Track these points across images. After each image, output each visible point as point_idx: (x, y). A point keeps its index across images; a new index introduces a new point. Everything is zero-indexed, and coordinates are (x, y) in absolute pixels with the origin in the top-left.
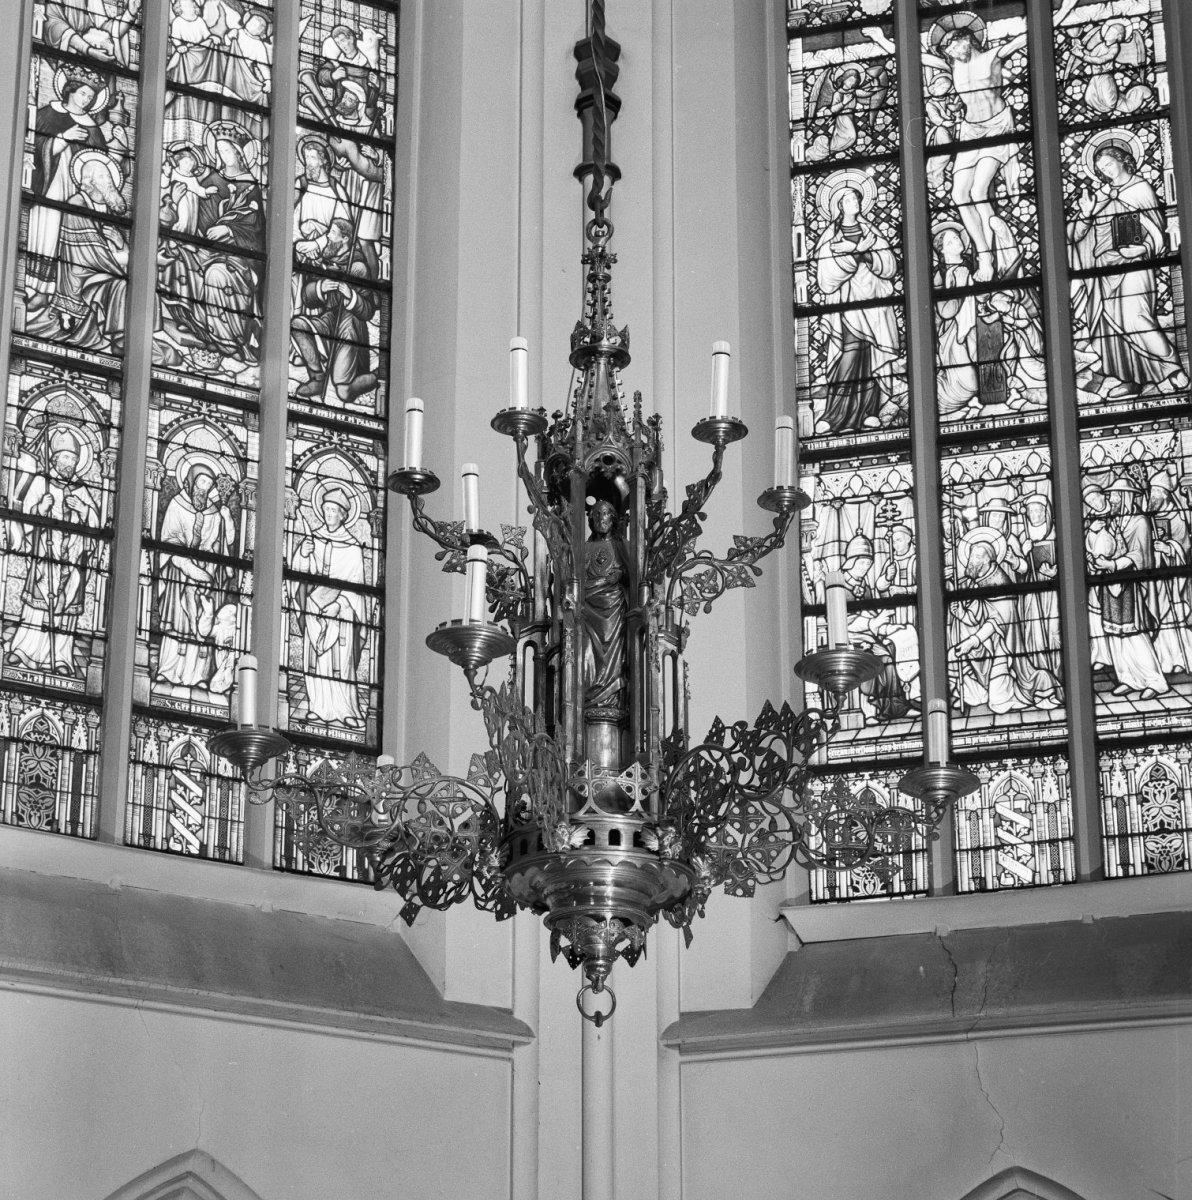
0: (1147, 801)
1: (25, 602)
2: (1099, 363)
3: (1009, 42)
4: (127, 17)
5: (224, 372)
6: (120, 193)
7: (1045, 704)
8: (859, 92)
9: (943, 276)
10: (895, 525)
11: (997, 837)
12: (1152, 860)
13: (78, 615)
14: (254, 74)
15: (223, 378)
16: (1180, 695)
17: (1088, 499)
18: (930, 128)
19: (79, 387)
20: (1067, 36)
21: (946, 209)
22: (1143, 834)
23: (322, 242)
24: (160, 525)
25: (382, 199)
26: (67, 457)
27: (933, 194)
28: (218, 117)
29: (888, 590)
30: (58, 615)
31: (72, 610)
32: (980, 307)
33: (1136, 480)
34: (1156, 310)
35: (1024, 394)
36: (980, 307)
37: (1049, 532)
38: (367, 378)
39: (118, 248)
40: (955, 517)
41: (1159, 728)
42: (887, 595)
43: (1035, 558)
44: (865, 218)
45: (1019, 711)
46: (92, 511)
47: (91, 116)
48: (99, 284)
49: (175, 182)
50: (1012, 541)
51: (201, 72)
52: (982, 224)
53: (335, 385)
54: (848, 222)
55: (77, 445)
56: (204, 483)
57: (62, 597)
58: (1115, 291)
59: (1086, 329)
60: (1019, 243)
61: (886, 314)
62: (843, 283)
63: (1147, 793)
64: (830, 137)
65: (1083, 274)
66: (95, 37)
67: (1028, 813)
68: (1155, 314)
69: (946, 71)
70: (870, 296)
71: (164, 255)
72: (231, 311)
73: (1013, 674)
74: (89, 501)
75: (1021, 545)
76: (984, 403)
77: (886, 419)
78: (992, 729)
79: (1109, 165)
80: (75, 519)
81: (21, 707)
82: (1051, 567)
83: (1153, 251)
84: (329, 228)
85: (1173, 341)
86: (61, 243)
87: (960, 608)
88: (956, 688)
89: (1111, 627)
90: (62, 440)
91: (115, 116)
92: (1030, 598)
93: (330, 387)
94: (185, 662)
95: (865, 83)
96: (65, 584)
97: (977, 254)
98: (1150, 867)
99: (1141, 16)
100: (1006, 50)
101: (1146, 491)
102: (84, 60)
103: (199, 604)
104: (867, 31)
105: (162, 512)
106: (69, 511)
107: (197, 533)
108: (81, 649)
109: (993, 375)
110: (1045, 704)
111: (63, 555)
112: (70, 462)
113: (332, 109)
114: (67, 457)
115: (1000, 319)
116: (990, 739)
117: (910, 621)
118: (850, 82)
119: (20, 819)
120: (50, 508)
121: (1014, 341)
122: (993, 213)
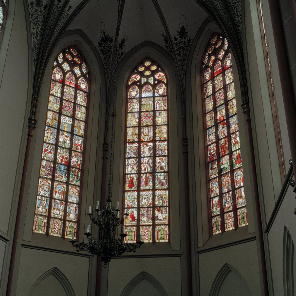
1: (40, 205)
4: (55, 138)
5: (63, 179)
7: (150, 220)
23: (74, 164)
34: (164, 177)
38: (78, 180)
43: (150, 204)
50: (148, 202)
51: (62, 144)
52: (147, 166)
54: (132, 164)
55: (46, 187)
56: (60, 191)
64: (130, 154)
65: (157, 173)
67: (148, 232)
68: (164, 178)
76: (146, 186)
80: (46, 196)
86: (46, 165)
90: (45, 187)
91: (53, 150)
100: (150, 147)
102: (49, 143)
103: (59, 205)
104: (135, 143)
106: (45, 195)
107: (59, 197)
109: (146, 183)
110: (150, 220)
112: (46, 189)
113: (76, 149)
115: (148, 177)
116: (144, 224)
118: (133, 148)
119: (38, 229)
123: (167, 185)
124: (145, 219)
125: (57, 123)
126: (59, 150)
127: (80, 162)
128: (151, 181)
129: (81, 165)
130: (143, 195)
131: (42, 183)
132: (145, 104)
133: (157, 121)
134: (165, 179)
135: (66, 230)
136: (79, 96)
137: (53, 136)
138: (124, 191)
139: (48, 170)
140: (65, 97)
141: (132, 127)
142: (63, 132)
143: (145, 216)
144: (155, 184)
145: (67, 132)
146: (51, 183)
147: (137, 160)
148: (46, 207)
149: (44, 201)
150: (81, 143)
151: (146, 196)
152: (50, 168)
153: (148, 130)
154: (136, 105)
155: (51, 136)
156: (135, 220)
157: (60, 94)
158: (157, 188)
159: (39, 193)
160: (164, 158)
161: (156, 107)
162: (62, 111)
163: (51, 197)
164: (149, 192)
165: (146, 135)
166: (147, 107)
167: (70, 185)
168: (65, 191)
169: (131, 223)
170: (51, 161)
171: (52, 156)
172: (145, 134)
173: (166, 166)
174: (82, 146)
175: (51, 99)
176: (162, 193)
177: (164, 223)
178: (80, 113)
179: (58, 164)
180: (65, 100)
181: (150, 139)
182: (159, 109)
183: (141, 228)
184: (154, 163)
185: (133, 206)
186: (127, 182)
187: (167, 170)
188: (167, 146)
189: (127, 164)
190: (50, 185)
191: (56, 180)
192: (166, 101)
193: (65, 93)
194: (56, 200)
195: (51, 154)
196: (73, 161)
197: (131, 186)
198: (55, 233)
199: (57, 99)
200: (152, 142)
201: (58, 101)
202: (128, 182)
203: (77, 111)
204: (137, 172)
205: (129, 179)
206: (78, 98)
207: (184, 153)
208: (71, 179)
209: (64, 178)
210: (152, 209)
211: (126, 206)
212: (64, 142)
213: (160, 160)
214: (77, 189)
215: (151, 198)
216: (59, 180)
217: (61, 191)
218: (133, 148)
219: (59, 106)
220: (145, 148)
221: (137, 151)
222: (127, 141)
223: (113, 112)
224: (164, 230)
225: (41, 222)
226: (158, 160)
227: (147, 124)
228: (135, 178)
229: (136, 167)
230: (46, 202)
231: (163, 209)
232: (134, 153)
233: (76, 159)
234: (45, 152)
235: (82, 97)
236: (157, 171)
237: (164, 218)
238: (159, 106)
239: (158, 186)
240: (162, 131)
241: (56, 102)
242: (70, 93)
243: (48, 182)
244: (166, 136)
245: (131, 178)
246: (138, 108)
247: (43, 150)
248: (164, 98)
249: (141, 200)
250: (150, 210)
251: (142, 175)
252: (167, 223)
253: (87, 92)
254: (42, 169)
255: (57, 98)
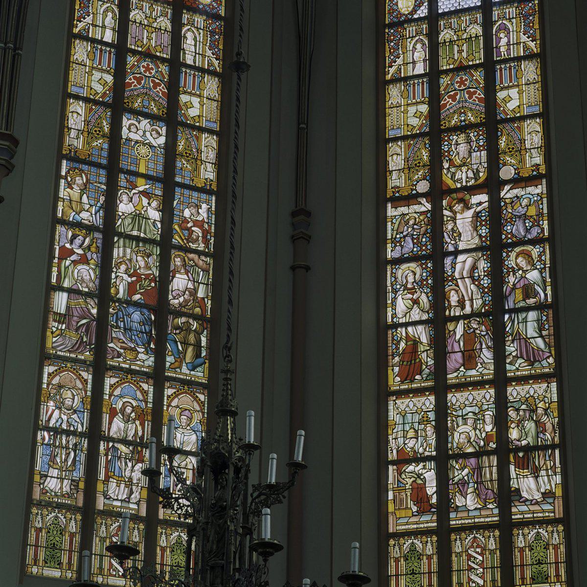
0: (533, 549)
2: (516, 352)
3: (480, 205)
4: (99, 205)
6: (94, 283)
7: (490, 506)
8: (415, 227)
9: (450, 311)
10: (427, 424)
11: (468, 564)
12: (534, 576)
13: (73, 471)
14: (154, 226)
15: (138, 363)
16: (548, 503)
17: (510, 414)
18: (446, 244)
19: (74, 369)
20: (505, 202)
21: (452, 281)
22: (531, 565)
23: (181, 299)
24: (109, 429)
25: (208, 279)
26: (69, 401)
27: (446, 273)
28: (137, 246)
29: (424, 453)
30: (64, 471)
31: (70, 469)
32: (465, 326)
33: (531, 405)
34: (541, 328)
35: (483, 365)
36: (465, 326)
37: (493, 428)
38: (199, 361)
39: (93, 307)
40: (453, 421)
41: (540, 517)
42: (423, 456)
44: (417, 284)
45: (480, 509)
46: (79, 424)
47: (83, 249)
48: (83, 324)
49: (118, 276)
50: (478, 432)
51: (131, 227)
52: (468, 288)
53: (186, 364)
54: (409, 286)
55: (74, 396)
56: (129, 410)
57: (66, 463)
58: (524, 319)
59: (510, 337)
60: (483, 296)
61: (425, 328)
62: (407, 313)
63: (533, 546)
64: (402, 247)
65: (510, 311)
66: (84, 215)
67: (481, 554)
68: (540, 330)
69: (453, 218)
70: (418, 319)
71: (113, 309)
72: (142, 333)
73: (477, 492)
74: (78, 420)
75: (481, 434)
77: (424, 376)
78: (469, 518)
79: (521, 261)
80: (72, 429)
81: (47, 513)
82: (494, 444)
83: (540, 301)
84: (185, 293)
85: (548, 343)
86: (68, 308)
87: (454, 462)
88: (452, 498)
89: (519, 471)
91: (93, 249)
92: (485, 458)
93: (184, 364)
94: (119, 490)
95: (419, 222)
96: (67, 457)
97: (465, 301)
98: (534, 579)
99: (538, 194)
101: (534, 411)
102: (78, 225)
104: (419, 200)
105: (110, 423)
106: (69, 424)
107: (126, 431)
108: (74, 486)
110: (490, 506)
111: (66, 444)
112: (70, 403)
114: (69, 401)
115: (474, 331)
116: (467, 521)
117: (432, 468)
118: (411, 222)
119: (46, 563)
120: (61, 423)
121: (480, 341)
122: (472, 282)
123: (551, 360)
124: (471, 501)
125: (106, 146)
126: (119, 247)
127: (207, 290)
128: (488, 347)
129: (210, 302)
130: (458, 403)
131: (56, 381)
132: (451, 41)
133: (502, 105)
134: (544, 333)
135: (159, 560)
136: (189, 35)
137: (92, 195)
138: (384, 394)
139: (77, 330)
140: (133, 40)
141: (404, 138)
142: (132, 178)
143: (470, 490)
144: (505, 357)
145: (147, 177)
146: (90, 377)
147: (429, 265)
148: (75, 474)
149: (67, 448)
150: (205, 215)
151: (469, 409)
152: (84, 321)
153: (469, 141)
154: (419, 46)
155: (85, 197)
156: (431, 506)
157: (113, 29)
158: (513, 374)
159: (44, 418)
160: (535, 251)
161: (498, 48)
162: (124, 98)
163: (95, 434)
164: (483, 392)
165: (460, 166)
166: (460, 52)
167: (167, 384)
168: (150, 405)
169: (417, 523)
170: (88, 295)
171: (91, 272)
172: (458, 161)
173: (544, 282)
174: (210, 227)
175: (80, 52)
176: (532, 393)
177: (547, 514)
178: (195, 101)
179: (114, 302)
180: (134, 53)
181: (476, 179)
182: (509, 54)
183: (456, 540)
184: (497, 273)
185: (421, 450)
186: (393, 358)
187: (549, 300)
188: (545, 200)
189: (392, 285)
190: (89, 386)
191: (168, 376)
192: (537, 16)
193: (134, 26)
194: (116, 445)
195: (89, 264)
196: (175, 287)
197: (411, 367)
198: (115, 576)
199: (101, 50)
200: (486, 190)
201: (108, 60)
202: (397, 359)
203: (185, 93)
204: (431, 315)
205: (402, 345)
206: (189, 43)
207: (293, 268)
208: (170, 359)
209: (142, 356)
210: (494, 460)
211: (395, 452)
212: (138, 217)
213: (520, 260)
214: (196, 399)
215: (489, 416)
216: (124, 366)
217: (133, 407)
218: (411, 222)
219: (109, 79)
220: (459, 216)
221: (429, 231)
222: (388, 197)
223: (239, 54)
224: (548, 544)
225: (55, 532)
226: (513, 259)
227: (463, 118)
228: (424, 339)
229: (427, 294)
230: (72, 454)
231: (539, 459)
232: (418, 239)
233: (189, 280)
234: (61, 259)
235: (201, 35)
236: (510, 304)
237: (545, 495)
238: (509, 41)
239: (517, 365)
240: (522, 141)
241: (100, 64)
242: (155, 25)
243: (80, 377)
244: (538, 160)
245: (407, 342)
246: (425, 61)
247: (52, 250)
248: (527, 8)
249: (449, 425)
250: (490, 466)
251: (451, 326)
252: (559, 514)
253: (222, 13)
254: (53, 325)
255: (104, 48)
